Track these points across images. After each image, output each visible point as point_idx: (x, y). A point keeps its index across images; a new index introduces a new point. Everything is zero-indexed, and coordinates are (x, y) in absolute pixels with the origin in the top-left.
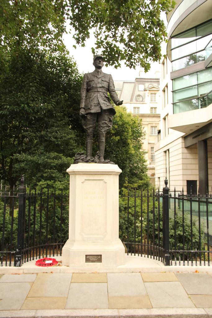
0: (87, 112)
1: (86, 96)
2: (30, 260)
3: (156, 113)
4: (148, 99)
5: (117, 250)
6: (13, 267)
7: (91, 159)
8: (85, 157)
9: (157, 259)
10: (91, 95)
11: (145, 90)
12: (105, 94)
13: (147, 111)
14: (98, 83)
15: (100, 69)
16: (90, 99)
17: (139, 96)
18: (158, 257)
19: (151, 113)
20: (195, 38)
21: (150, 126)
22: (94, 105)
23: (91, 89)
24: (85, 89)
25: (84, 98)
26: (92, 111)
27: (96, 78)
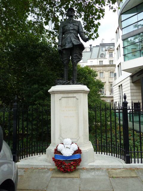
0: (63, 48)
2: (25, 158)
11: (106, 50)
17: (102, 54)
18: (115, 155)
20: (137, 13)
21: (109, 72)
26: (67, 47)
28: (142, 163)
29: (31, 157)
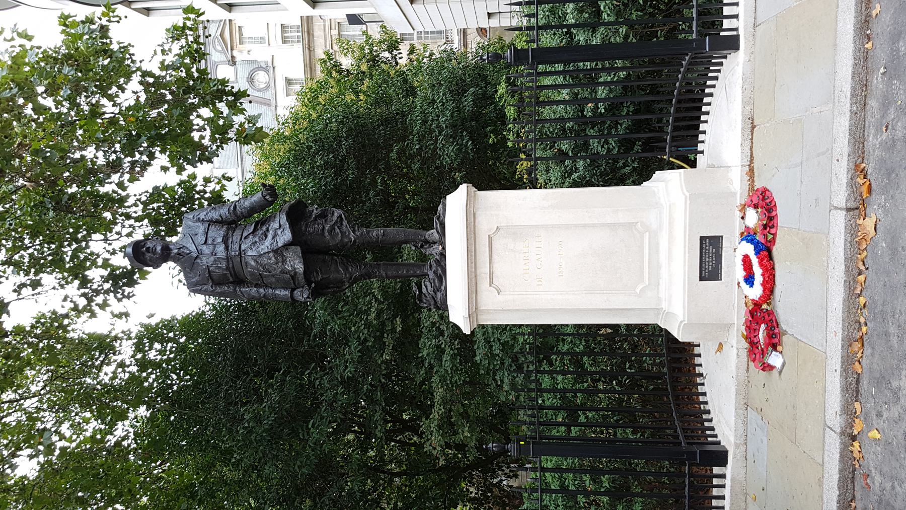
1: (257, 286)
3: (298, 27)
4: (260, 54)
5: (688, 194)
6: (728, 470)
7: (434, 269)
8: (428, 284)
9: (714, 86)
10: (252, 274)
11: (233, 62)
12: (245, 234)
13: (296, 52)
14: (213, 253)
15: (172, 247)
16: (266, 276)
18: (709, 83)
19: (298, 41)
22: (280, 264)
23: (235, 274)
24: (235, 289)
25: (262, 291)
26: (300, 267)
27: (198, 261)
28: (737, 4)
29: (707, 398)
